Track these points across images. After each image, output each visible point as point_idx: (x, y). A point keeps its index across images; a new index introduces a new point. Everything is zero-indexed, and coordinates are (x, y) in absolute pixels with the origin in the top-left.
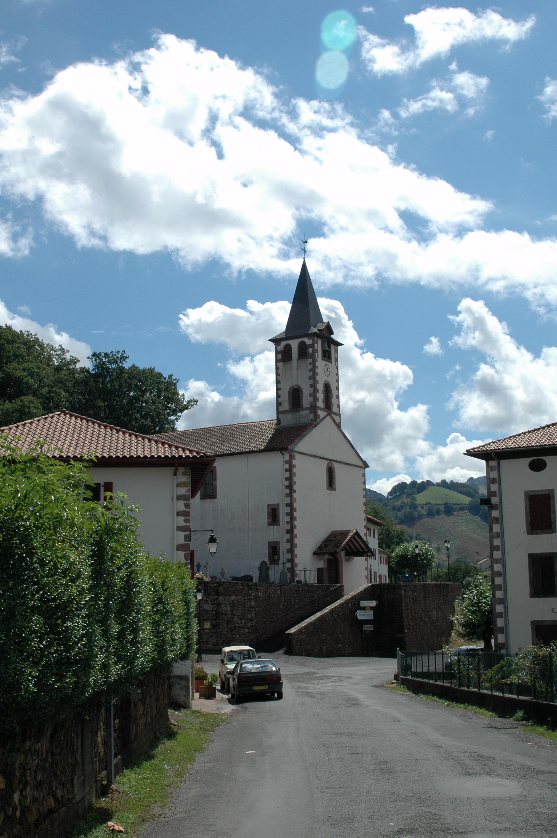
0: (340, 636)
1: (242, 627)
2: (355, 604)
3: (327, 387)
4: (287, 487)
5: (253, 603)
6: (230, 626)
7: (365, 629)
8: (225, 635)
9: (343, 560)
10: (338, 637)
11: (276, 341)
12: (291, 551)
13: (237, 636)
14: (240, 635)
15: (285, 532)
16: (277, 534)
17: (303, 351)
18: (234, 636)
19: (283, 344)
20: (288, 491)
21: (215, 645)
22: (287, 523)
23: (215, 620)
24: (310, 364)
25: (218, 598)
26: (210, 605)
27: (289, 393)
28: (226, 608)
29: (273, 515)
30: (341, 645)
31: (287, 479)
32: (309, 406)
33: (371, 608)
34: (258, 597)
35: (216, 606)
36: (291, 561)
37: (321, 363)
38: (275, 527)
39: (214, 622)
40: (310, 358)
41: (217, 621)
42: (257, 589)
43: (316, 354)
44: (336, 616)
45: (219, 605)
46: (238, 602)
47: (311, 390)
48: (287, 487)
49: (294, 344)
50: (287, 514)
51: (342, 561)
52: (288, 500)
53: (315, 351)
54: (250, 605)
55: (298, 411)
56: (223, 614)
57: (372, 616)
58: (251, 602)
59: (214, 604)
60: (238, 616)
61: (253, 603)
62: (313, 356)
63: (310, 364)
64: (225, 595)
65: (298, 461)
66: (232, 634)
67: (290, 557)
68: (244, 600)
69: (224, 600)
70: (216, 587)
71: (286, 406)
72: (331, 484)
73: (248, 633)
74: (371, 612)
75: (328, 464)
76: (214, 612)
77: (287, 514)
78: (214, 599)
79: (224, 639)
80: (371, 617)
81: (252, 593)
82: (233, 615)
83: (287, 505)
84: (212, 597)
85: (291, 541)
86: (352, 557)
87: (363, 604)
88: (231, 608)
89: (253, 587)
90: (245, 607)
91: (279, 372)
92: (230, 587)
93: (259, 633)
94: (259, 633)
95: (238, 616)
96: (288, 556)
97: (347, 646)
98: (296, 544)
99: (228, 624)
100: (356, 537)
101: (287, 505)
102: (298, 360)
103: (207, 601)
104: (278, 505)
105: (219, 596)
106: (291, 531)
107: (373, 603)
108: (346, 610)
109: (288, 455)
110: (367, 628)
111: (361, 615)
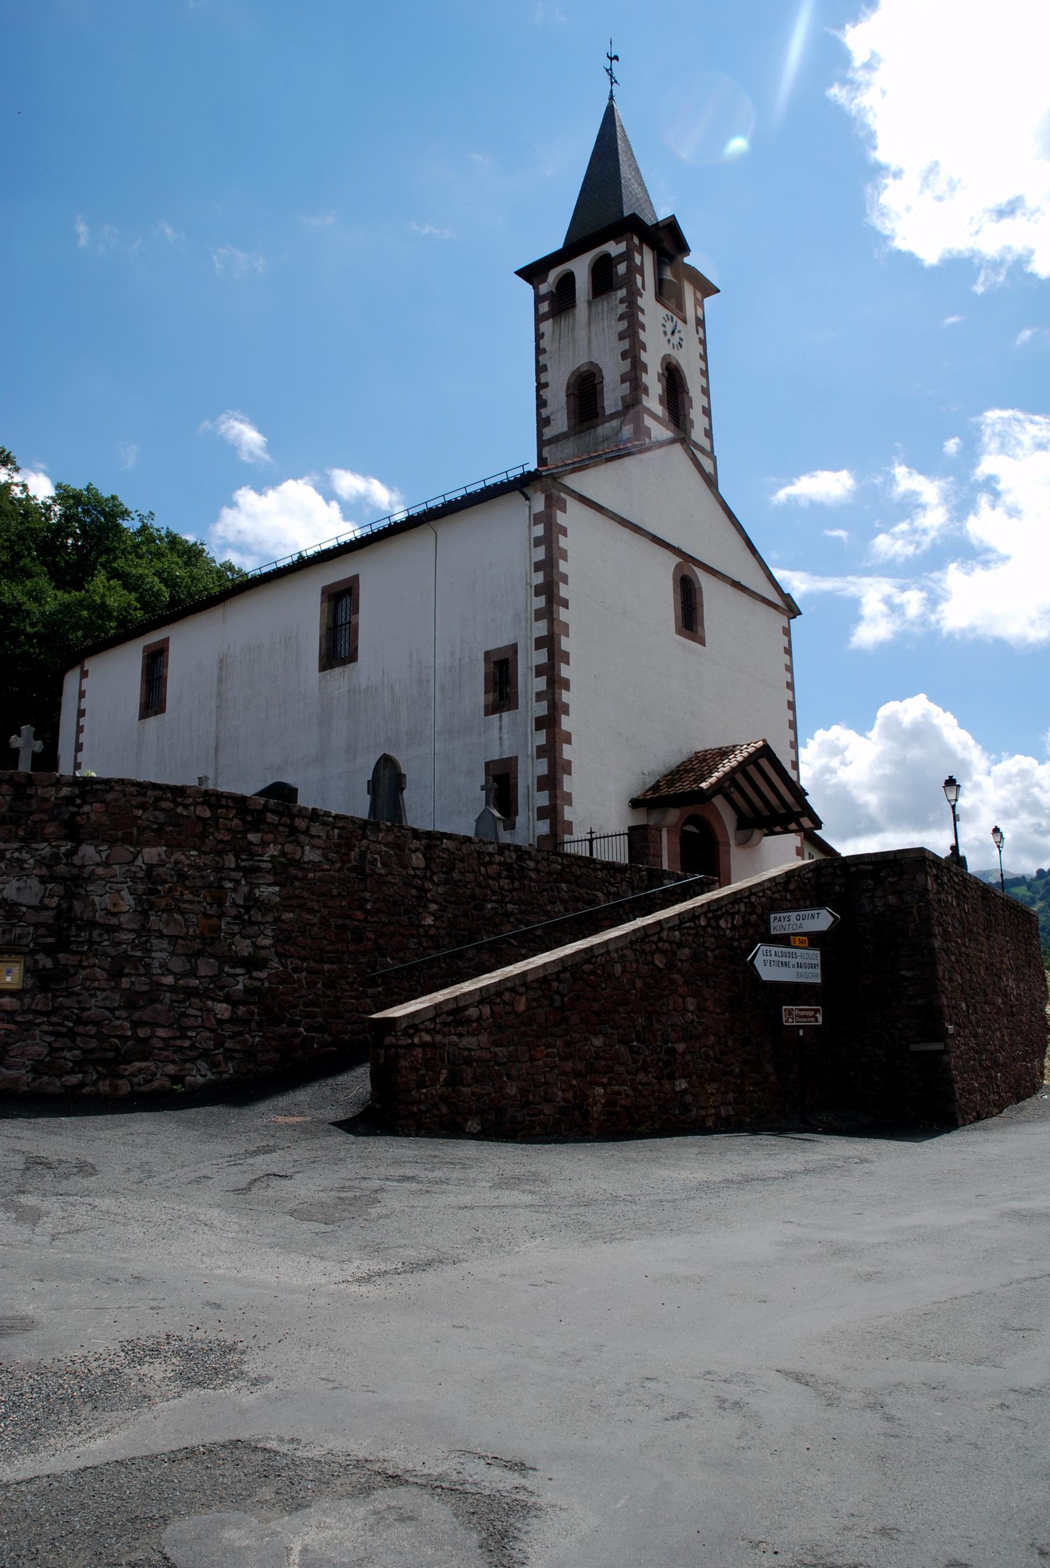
0: (681, 1047)
1: (191, 993)
2: (746, 924)
3: (673, 379)
4: (538, 591)
5: (268, 891)
6: (125, 982)
7: (788, 1022)
8: (96, 1023)
9: (732, 842)
10: (672, 1051)
11: (532, 273)
12: (550, 782)
13: (161, 1032)
14: (183, 1029)
15: (531, 725)
16: (513, 736)
17: (604, 278)
18: (142, 1033)
19: (554, 275)
20: (540, 602)
21: (38, 1069)
22: (539, 696)
23: (50, 951)
24: (622, 301)
25: (73, 852)
26: (34, 882)
27: (568, 388)
28: (114, 898)
29: (501, 674)
30: (682, 1084)
31: (538, 567)
32: (620, 408)
33: (815, 940)
34: (298, 864)
35: (59, 889)
36: (551, 813)
37: (652, 312)
38: (505, 715)
39: (45, 961)
40: (620, 288)
41: (62, 957)
42: (293, 831)
43: (639, 278)
44: (659, 961)
45: (75, 883)
46: (182, 877)
47: (626, 366)
48: (538, 591)
49: (581, 267)
50: (540, 671)
51: (729, 845)
52: (541, 629)
53: (636, 269)
54: (250, 896)
55: (590, 428)
56: (92, 924)
57: (818, 971)
58: (253, 886)
59: (54, 878)
60: (173, 939)
61: (268, 891)
62: (628, 281)
63: (622, 301)
64: (112, 842)
65: (572, 517)
66: (137, 1024)
67: (546, 802)
68: (219, 869)
69: (107, 864)
70: (69, 800)
71: (561, 423)
72: (689, 619)
73: (231, 1021)
74: (814, 956)
75: (678, 567)
76: (46, 916)
77: (540, 671)
78: (56, 857)
79: (93, 1044)
80: (814, 976)
81: (264, 844)
82: (144, 930)
83: (540, 643)
84: (45, 849)
85: (550, 751)
86: (757, 833)
87: (783, 923)
88: (139, 900)
89: (271, 818)
90: (220, 903)
91: (543, 344)
92: (143, 806)
93: (293, 1024)
94: (293, 1024)
95: (173, 939)
96: (542, 799)
97: (711, 1088)
98: (569, 763)
99: (116, 973)
100: (764, 763)
101: (540, 643)
102: (589, 303)
103: (21, 862)
104: (514, 647)
105: (79, 843)
106: (549, 723)
107: (822, 920)
108: (710, 942)
109: (543, 495)
110: (797, 1017)
111: (771, 965)
